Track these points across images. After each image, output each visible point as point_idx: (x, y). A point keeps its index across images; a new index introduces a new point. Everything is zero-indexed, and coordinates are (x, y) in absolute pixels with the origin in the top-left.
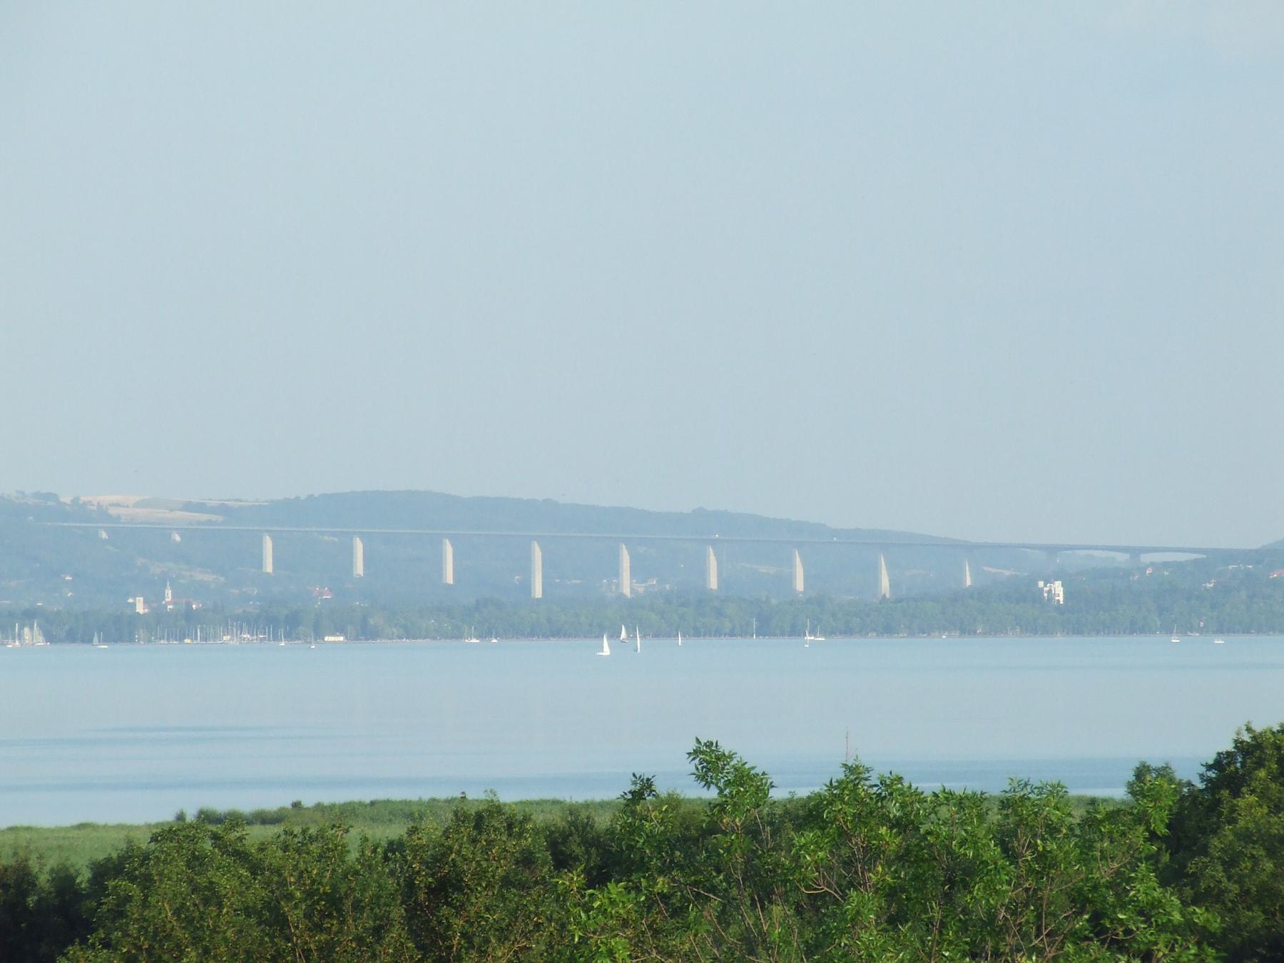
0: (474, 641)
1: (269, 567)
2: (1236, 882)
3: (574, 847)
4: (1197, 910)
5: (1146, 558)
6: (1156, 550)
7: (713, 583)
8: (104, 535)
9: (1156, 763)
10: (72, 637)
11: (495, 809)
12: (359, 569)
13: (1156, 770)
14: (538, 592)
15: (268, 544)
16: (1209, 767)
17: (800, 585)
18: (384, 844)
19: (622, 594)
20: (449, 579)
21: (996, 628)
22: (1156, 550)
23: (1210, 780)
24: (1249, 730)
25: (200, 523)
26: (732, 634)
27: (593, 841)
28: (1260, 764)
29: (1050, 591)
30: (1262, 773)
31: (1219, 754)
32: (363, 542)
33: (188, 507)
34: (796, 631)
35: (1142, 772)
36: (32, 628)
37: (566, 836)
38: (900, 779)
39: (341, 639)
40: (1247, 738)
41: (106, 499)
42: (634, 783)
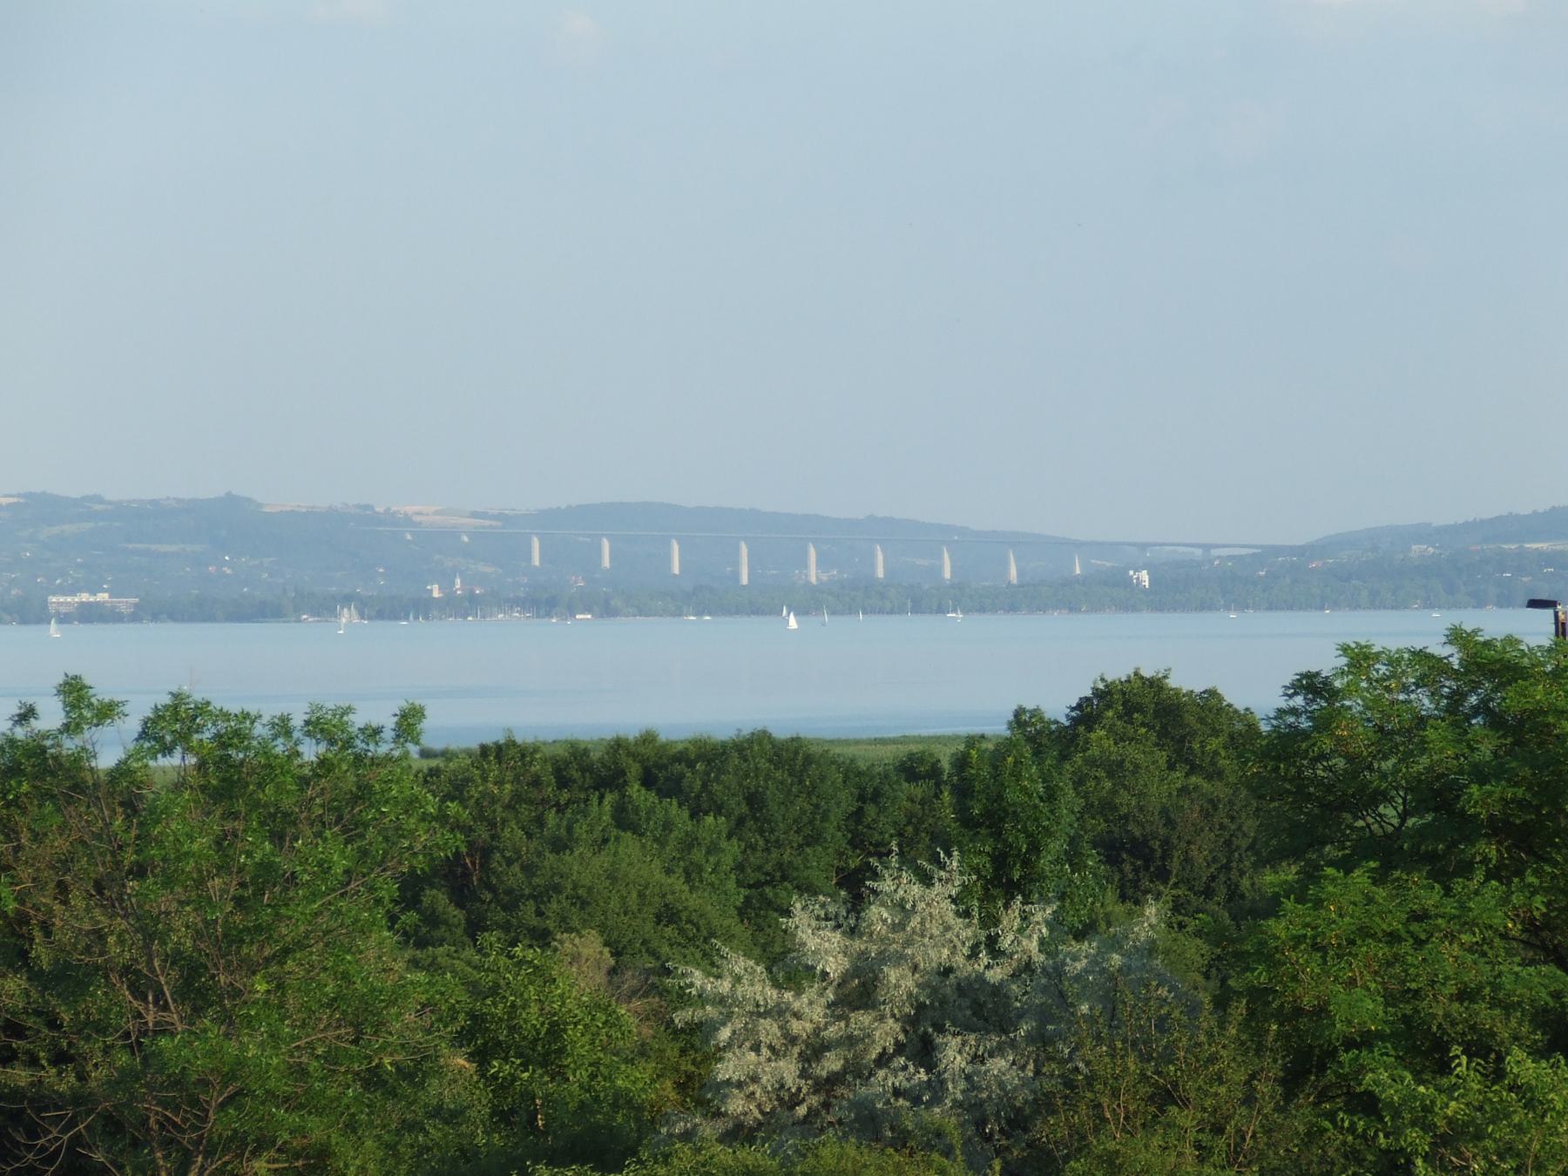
0: (708, 618)
1: (536, 561)
2: (1082, 798)
3: (574, 773)
4: (450, 805)
5: (1215, 552)
6: (1217, 546)
7: (880, 573)
8: (409, 537)
9: (1030, 706)
10: (380, 615)
11: (512, 743)
12: (606, 563)
13: (1030, 711)
14: (745, 580)
15: (536, 543)
16: (1073, 709)
17: (947, 575)
18: (425, 771)
19: (808, 582)
20: (676, 571)
21: (1097, 607)
22: (1217, 546)
23: (1073, 718)
24: (1103, 680)
25: (484, 527)
26: (891, 612)
27: (586, 769)
28: (1109, 707)
29: (1138, 578)
30: (1110, 713)
31: (1081, 699)
32: (609, 541)
33: (474, 515)
34: (941, 610)
35: (1019, 713)
36: (349, 609)
37: (567, 764)
38: (208, 703)
39: (589, 616)
40: (1101, 686)
41: (410, 509)
42: (20, 708)
